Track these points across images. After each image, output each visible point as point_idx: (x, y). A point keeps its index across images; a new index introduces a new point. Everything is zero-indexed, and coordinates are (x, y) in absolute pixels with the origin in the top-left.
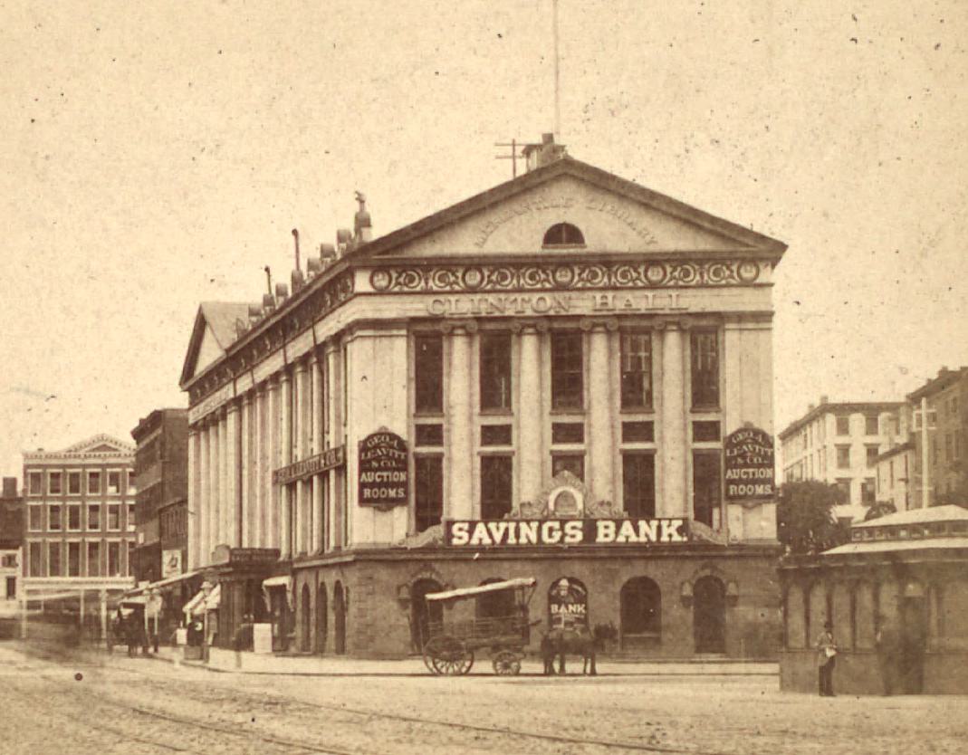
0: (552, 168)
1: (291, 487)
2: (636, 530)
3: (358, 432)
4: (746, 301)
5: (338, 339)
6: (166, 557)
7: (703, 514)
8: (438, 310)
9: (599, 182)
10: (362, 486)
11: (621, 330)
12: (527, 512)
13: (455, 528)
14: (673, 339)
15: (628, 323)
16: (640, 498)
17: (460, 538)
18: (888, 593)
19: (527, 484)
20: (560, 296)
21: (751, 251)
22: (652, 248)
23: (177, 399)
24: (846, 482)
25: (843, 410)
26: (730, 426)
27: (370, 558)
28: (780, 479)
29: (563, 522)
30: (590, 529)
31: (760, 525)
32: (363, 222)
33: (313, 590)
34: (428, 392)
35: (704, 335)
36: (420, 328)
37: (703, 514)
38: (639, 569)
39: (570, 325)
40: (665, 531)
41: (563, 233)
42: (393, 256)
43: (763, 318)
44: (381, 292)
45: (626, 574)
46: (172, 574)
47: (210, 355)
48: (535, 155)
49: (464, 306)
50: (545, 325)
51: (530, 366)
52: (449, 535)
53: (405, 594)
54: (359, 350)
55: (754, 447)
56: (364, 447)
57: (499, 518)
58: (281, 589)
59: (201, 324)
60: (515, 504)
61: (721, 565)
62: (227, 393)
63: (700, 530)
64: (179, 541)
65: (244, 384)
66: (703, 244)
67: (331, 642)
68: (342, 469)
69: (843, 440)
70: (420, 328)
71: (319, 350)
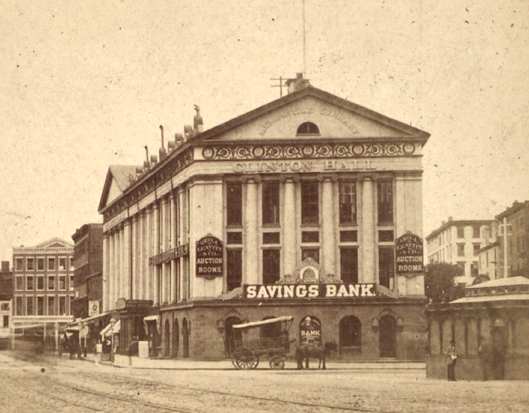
0: (302, 92)
1: (159, 266)
2: (348, 290)
3: (195, 236)
4: (408, 164)
5: (185, 185)
6: (91, 305)
7: (384, 281)
8: (239, 170)
9: (328, 100)
10: (198, 266)
11: (340, 181)
12: (288, 280)
13: (249, 289)
14: (368, 185)
15: (343, 177)
16: (350, 272)
17: (251, 294)
18: (486, 324)
19: (288, 265)
20: (306, 162)
21: (410, 138)
22: (356, 136)
23: (97, 218)
24: (462, 264)
25: (461, 224)
26: (399, 233)
27: (202, 305)
28: (426, 262)
29: (308, 286)
30: (322, 289)
31: (415, 287)
32: (198, 121)
33: (171, 323)
34: (234, 214)
35: (385, 183)
36: (229, 179)
37: (384, 281)
38: (349, 312)
39: (312, 178)
40: (364, 291)
41: (308, 128)
42: (215, 140)
43: (417, 174)
44: (208, 160)
45: (342, 314)
46: (94, 314)
47: (115, 194)
48: (292, 85)
49: (254, 167)
50: (298, 178)
51: (290, 200)
52: (246, 293)
53: (221, 325)
54: (196, 191)
55: (412, 244)
56: (199, 245)
57: (273, 284)
58: (153, 322)
59: (110, 177)
60: (282, 276)
61: (394, 309)
62: (124, 215)
63: (383, 290)
64: (98, 296)
65: (133, 210)
66: (385, 133)
67: (181, 351)
68: (187, 257)
69: (461, 241)
70: (229, 179)
71: (175, 191)
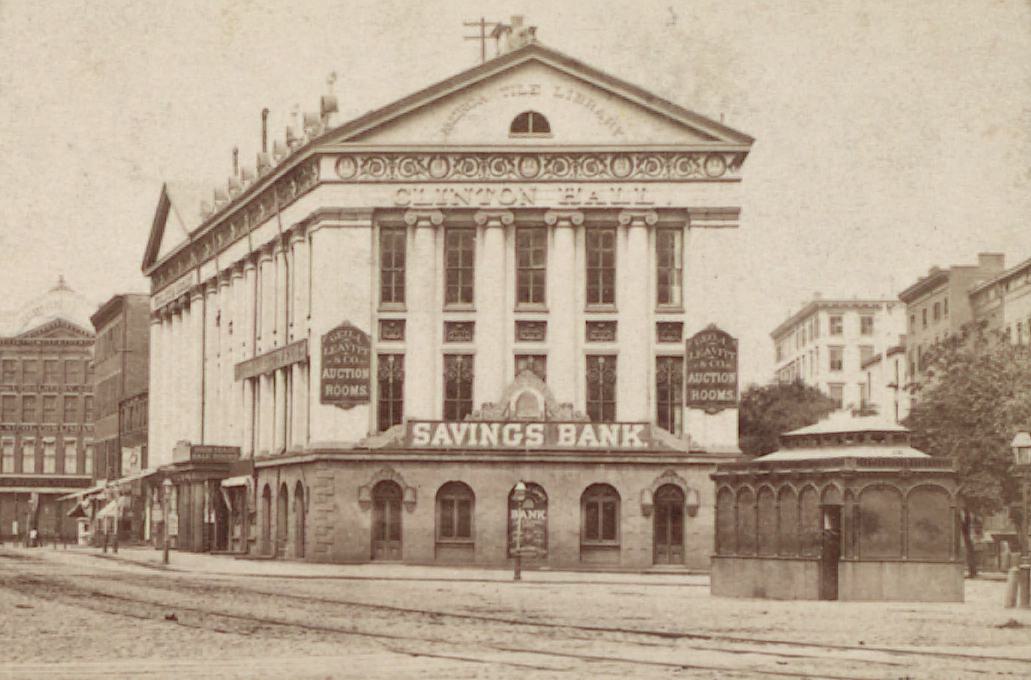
5: (303, 226)
7: (665, 419)
9: (572, 69)
17: (421, 439)
19: (490, 384)
40: (627, 436)
50: (510, 218)
52: (409, 435)
53: (366, 496)
58: (242, 488)
59: (165, 206)
60: (477, 406)
68: (306, 364)
71: (286, 237)
